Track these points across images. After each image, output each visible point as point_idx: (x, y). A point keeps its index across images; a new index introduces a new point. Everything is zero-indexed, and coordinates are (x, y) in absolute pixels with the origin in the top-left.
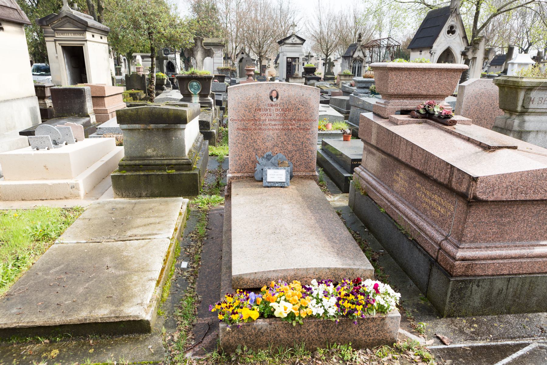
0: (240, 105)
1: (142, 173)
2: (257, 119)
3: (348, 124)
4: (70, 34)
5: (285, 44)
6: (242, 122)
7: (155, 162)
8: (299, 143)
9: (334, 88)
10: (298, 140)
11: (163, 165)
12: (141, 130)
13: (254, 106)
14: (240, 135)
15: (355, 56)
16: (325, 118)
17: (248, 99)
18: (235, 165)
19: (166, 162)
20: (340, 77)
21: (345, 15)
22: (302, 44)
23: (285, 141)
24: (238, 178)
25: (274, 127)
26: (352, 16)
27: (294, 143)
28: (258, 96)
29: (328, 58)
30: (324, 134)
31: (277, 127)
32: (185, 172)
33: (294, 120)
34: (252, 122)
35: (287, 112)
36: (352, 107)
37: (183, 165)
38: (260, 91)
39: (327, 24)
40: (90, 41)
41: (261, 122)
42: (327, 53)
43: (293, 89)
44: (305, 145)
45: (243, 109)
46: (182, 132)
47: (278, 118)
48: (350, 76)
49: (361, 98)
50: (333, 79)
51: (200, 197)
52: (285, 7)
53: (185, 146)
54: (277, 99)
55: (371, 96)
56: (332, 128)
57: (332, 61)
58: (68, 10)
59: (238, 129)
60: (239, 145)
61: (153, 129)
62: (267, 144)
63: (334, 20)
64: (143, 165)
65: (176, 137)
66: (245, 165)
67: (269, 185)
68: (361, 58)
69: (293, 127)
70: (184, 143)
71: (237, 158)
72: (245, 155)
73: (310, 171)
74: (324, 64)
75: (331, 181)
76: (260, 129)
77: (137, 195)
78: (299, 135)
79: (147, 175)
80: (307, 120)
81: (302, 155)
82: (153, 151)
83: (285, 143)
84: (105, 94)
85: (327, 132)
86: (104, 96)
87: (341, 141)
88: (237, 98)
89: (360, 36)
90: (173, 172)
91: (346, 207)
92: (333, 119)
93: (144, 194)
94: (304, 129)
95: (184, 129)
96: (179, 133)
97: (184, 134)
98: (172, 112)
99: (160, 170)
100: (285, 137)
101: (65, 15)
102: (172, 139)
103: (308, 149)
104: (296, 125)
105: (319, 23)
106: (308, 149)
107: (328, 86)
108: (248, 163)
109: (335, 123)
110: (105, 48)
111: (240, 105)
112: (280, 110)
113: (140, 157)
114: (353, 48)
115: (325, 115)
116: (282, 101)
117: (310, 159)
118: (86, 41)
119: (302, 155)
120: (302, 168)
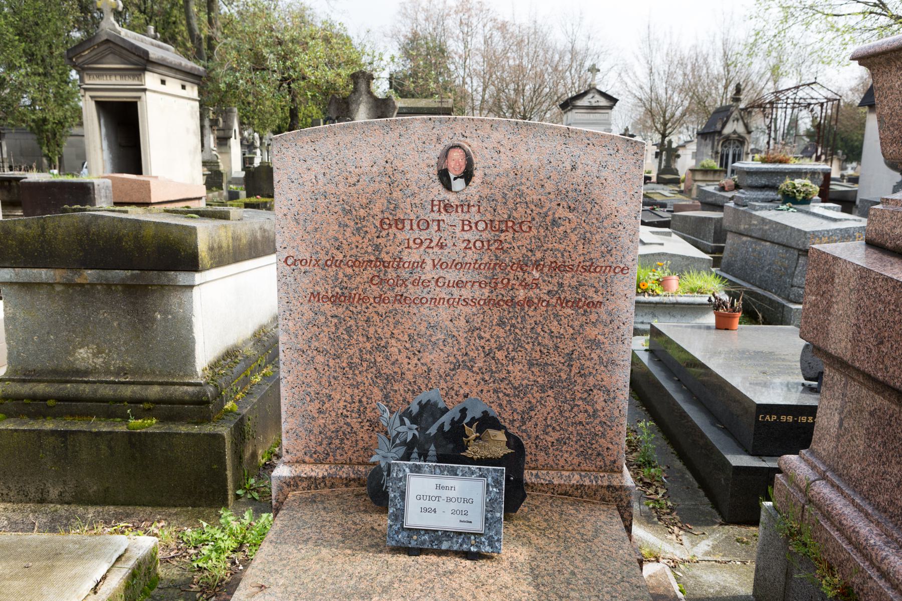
0: (323, 203)
1: (49, 426)
2: (387, 258)
3: (724, 278)
4: (113, 78)
5: (575, 107)
6: (332, 271)
7: (96, 391)
8: (555, 358)
9: (679, 196)
10: (551, 344)
11: (121, 400)
12: (59, 288)
13: (376, 210)
14: (323, 319)
15: (727, 130)
16: (660, 261)
17: (352, 180)
18: (303, 434)
19: (128, 391)
20: (693, 175)
21: (704, 52)
22: (611, 108)
23: (500, 348)
24: (314, 482)
25: (455, 291)
26: (720, 54)
27: (537, 355)
28: (389, 170)
29: (667, 139)
30: (657, 303)
31: (466, 293)
32: (183, 429)
33: (537, 265)
34: (370, 272)
35: (510, 235)
36: (729, 236)
37: (182, 402)
38: (400, 150)
39: (664, 71)
40: (154, 92)
41: (404, 274)
42: (665, 130)
43: (532, 144)
44: (582, 367)
45: (332, 219)
46: (185, 296)
47: (471, 256)
48: (715, 172)
49: (757, 213)
50: (676, 182)
51: (227, 516)
52: (579, 46)
53: (194, 342)
54: (467, 184)
55: (784, 207)
56: (680, 288)
57: (674, 145)
58: (112, 27)
59: (315, 295)
60: (320, 359)
61: (92, 285)
62: (427, 357)
63: (682, 63)
64: (59, 399)
65: (165, 313)
66: (343, 435)
67: (413, 544)
68: (740, 136)
69: (531, 294)
70: (190, 331)
71: (313, 407)
72: (341, 396)
73: (600, 469)
74: (658, 155)
75: (678, 464)
76: (401, 299)
77: (32, 496)
78: (554, 326)
79: (64, 434)
80: (590, 267)
81: (567, 407)
82: (95, 355)
83: (500, 355)
84: (150, 197)
85: (666, 299)
86: (147, 201)
87: (708, 328)
88: (308, 176)
89: (738, 90)
90: (149, 425)
91: (748, 596)
92: (681, 265)
93: (54, 493)
94: (575, 304)
95: (192, 287)
96: (174, 299)
97: (191, 303)
98: (150, 232)
99: (109, 415)
100: (501, 332)
101: (105, 38)
102: (155, 319)
103: (591, 381)
104: (545, 289)
105: (648, 71)
106: (591, 381)
107: (666, 193)
108: (356, 426)
109: (687, 276)
110: (192, 107)
111: (323, 203)
112: (481, 226)
113: (55, 372)
114: (722, 115)
115: (659, 254)
116: (486, 191)
117: (602, 423)
118: (145, 90)
119: (567, 407)
120: (568, 455)
